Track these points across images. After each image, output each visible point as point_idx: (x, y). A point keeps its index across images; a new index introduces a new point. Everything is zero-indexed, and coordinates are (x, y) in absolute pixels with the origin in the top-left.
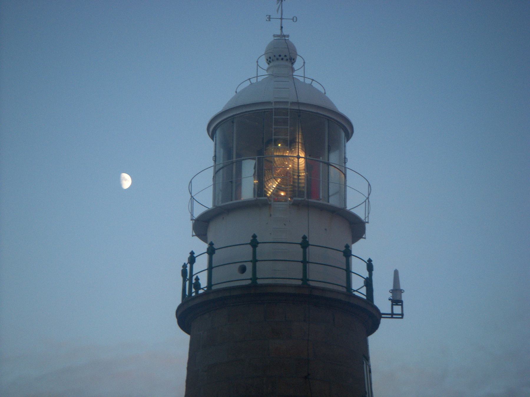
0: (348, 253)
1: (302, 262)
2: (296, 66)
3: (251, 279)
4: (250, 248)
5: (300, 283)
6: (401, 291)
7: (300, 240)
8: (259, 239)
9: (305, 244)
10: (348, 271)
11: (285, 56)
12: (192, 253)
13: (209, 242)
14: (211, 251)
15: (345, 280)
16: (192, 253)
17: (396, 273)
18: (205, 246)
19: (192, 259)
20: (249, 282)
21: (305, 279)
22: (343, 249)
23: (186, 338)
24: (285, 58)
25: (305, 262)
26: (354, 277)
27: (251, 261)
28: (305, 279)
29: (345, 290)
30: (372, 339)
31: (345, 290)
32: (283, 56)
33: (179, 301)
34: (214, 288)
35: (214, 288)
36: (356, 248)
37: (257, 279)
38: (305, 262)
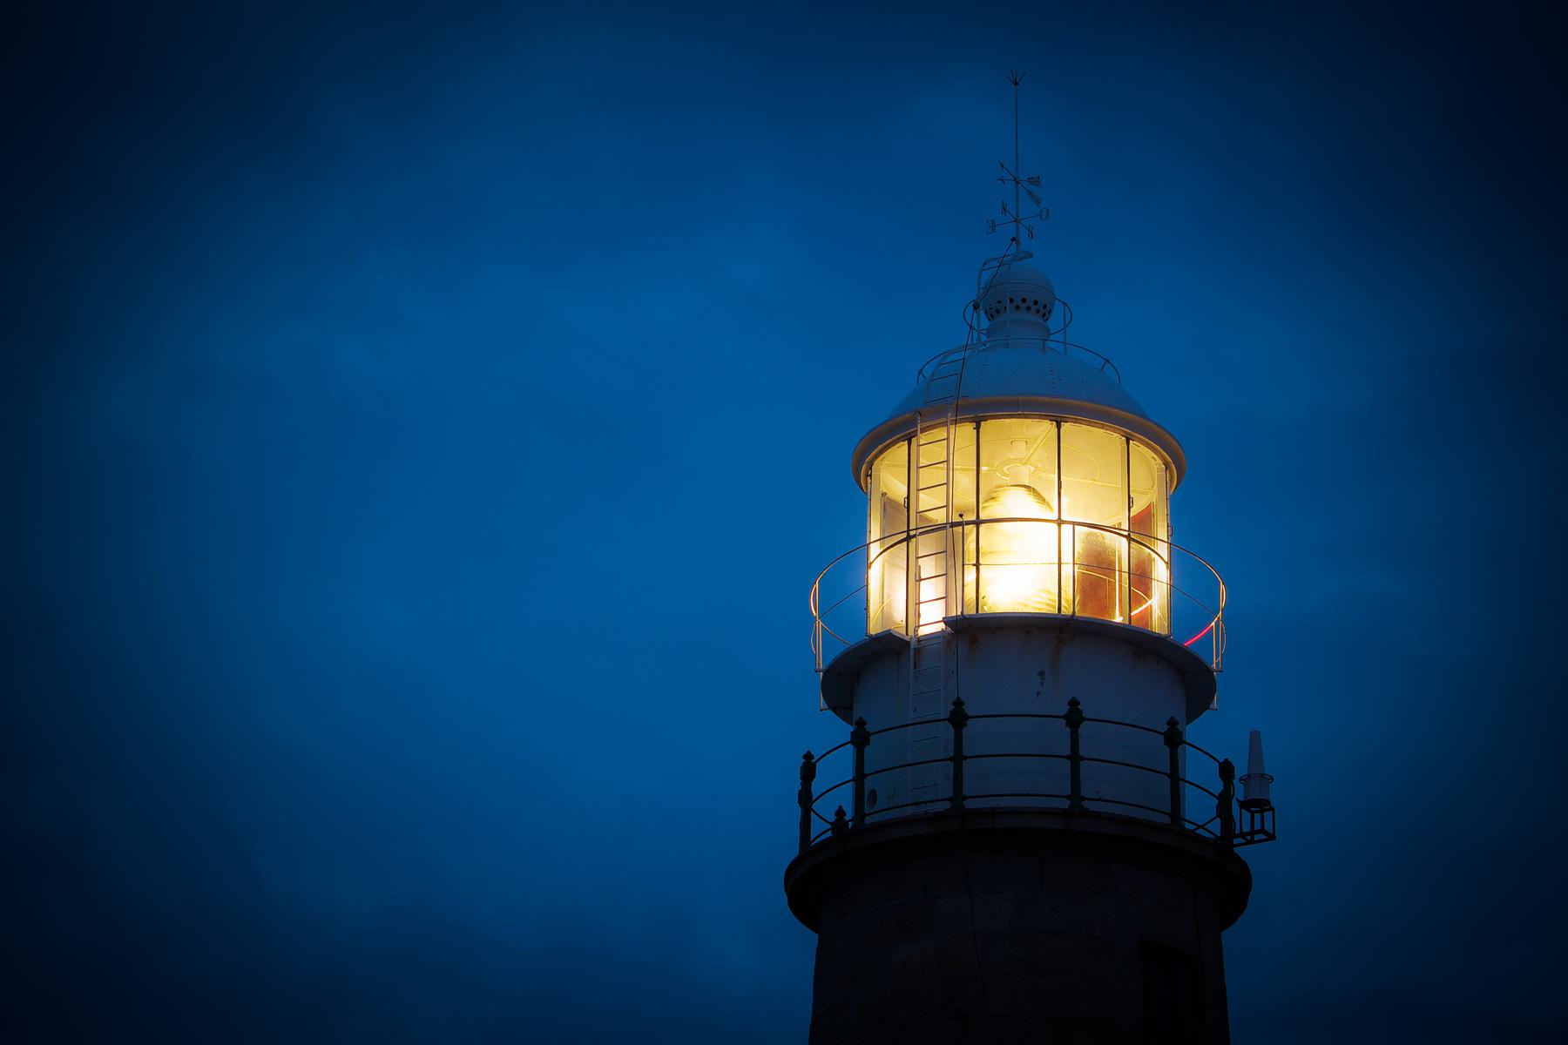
0: (1173, 738)
1: (1068, 757)
2: (1054, 322)
3: (950, 799)
4: (948, 730)
5: (1065, 804)
6: (1265, 779)
7: (1063, 709)
8: (968, 709)
9: (1074, 717)
10: (1175, 778)
11: (1036, 303)
12: (808, 756)
13: (855, 718)
14: (860, 739)
15: (1169, 798)
16: (808, 756)
17: (1255, 737)
18: (845, 730)
19: (808, 770)
20: (948, 805)
21: (1075, 794)
22: (1164, 728)
23: (808, 940)
24: (1034, 308)
25: (1075, 758)
26: (1189, 792)
27: (951, 759)
28: (1075, 794)
29: (1167, 820)
30: (1225, 935)
31: (1167, 820)
32: (1030, 303)
33: (793, 852)
34: (868, 820)
35: (868, 820)
36: (1192, 732)
37: (965, 798)
38: (1075, 758)
